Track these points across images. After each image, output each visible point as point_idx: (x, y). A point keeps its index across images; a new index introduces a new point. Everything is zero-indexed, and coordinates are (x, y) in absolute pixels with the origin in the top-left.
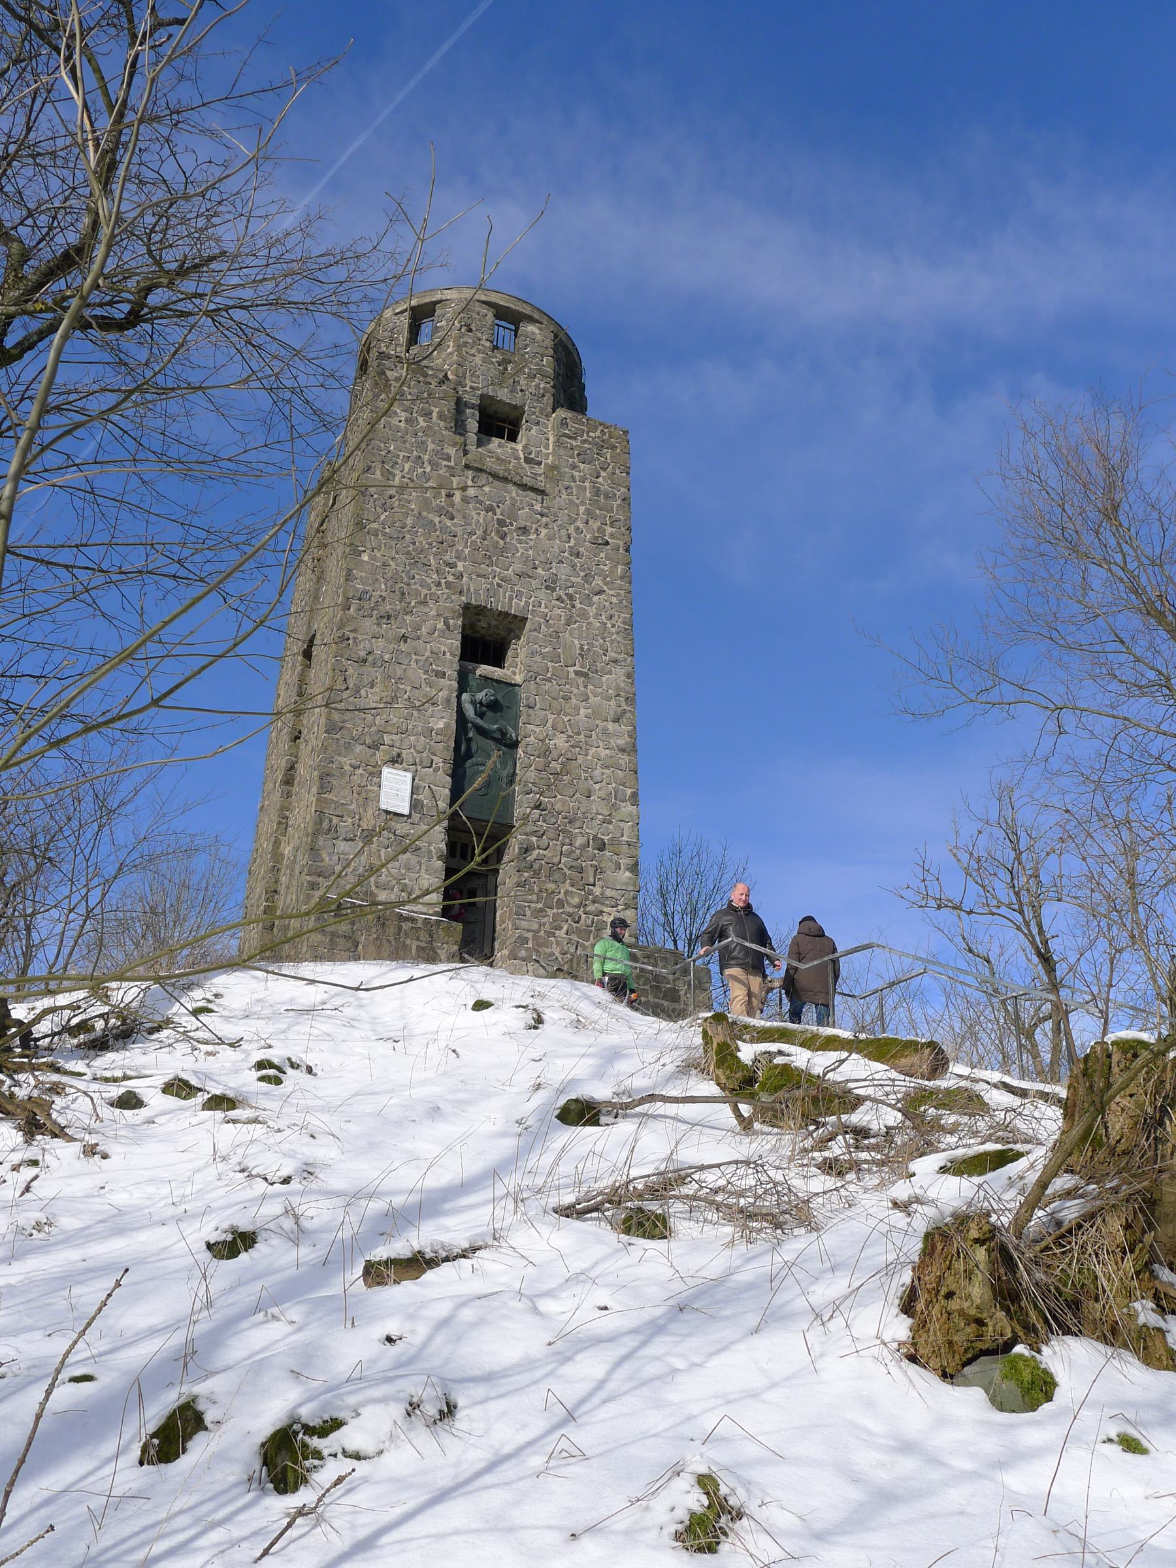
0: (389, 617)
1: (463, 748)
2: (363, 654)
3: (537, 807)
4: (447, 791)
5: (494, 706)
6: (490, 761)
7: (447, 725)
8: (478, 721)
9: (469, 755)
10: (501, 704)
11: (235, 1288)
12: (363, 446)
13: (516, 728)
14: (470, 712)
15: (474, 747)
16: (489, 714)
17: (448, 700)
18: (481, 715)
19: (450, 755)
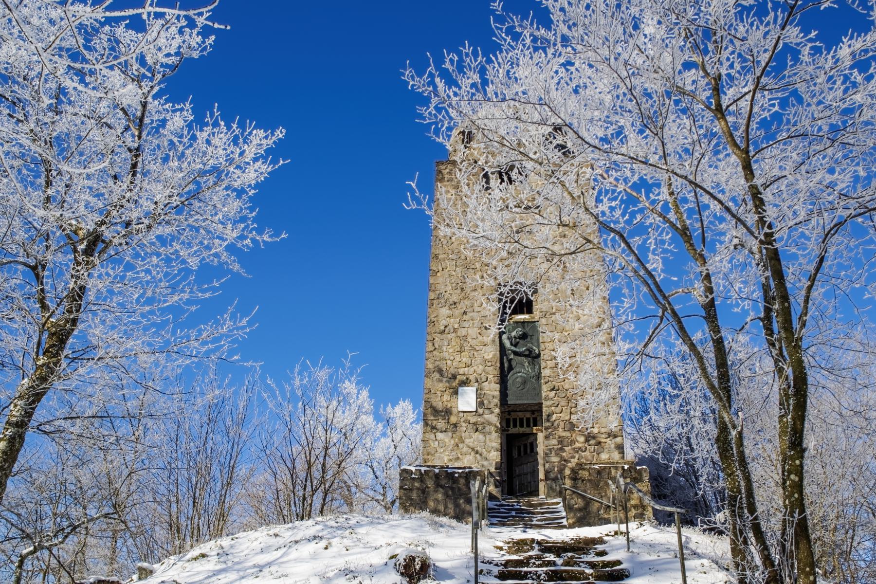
0: (455, 304)
1: (506, 365)
2: (442, 328)
3: (552, 390)
4: (498, 393)
5: (524, 336)
6: (522, 370)
7: (494, 356)
8: (513, 348)
9: (511, 368)
10: (528, 333)
11: (266, 565)
12: (223, 498)
13: (538, 346)
14: (507, 344)
15: (514, 363)
16: (521, 342)
17: (494, 341)
18: (516, 345)
19: (497, 372)
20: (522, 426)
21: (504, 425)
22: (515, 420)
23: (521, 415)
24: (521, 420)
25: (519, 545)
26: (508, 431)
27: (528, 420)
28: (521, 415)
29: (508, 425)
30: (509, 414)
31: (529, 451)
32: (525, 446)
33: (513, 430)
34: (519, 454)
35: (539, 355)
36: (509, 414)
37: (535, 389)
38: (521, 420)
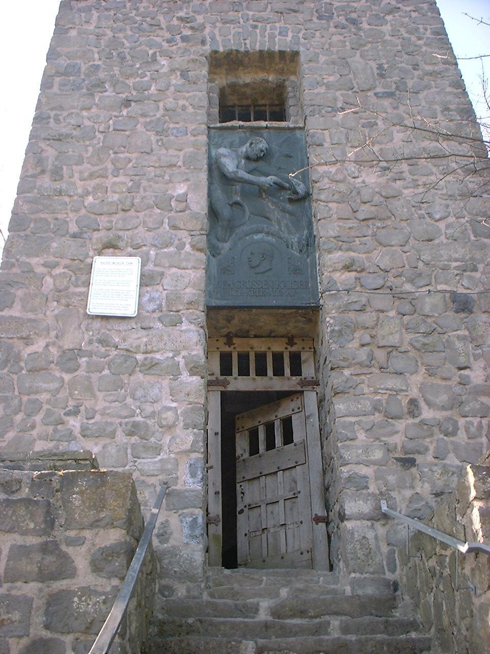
3: (348, 268)
20: (261, 372)
21: (216, 368)
22: (244, 358)
23: (259, 346)
24: (261, 358)
25: (254, 617)
26: (225, 384)
27: (278, 358)
28: (259, 346)
29: (226, 370)
30: (229, 343)
31: (262, 436)
32: (270, 428)
33: (239, 384)
34: (254, 450)
35: (307, 196)
36: (229, 343)
37: (297, 271)
38: (261, 358)
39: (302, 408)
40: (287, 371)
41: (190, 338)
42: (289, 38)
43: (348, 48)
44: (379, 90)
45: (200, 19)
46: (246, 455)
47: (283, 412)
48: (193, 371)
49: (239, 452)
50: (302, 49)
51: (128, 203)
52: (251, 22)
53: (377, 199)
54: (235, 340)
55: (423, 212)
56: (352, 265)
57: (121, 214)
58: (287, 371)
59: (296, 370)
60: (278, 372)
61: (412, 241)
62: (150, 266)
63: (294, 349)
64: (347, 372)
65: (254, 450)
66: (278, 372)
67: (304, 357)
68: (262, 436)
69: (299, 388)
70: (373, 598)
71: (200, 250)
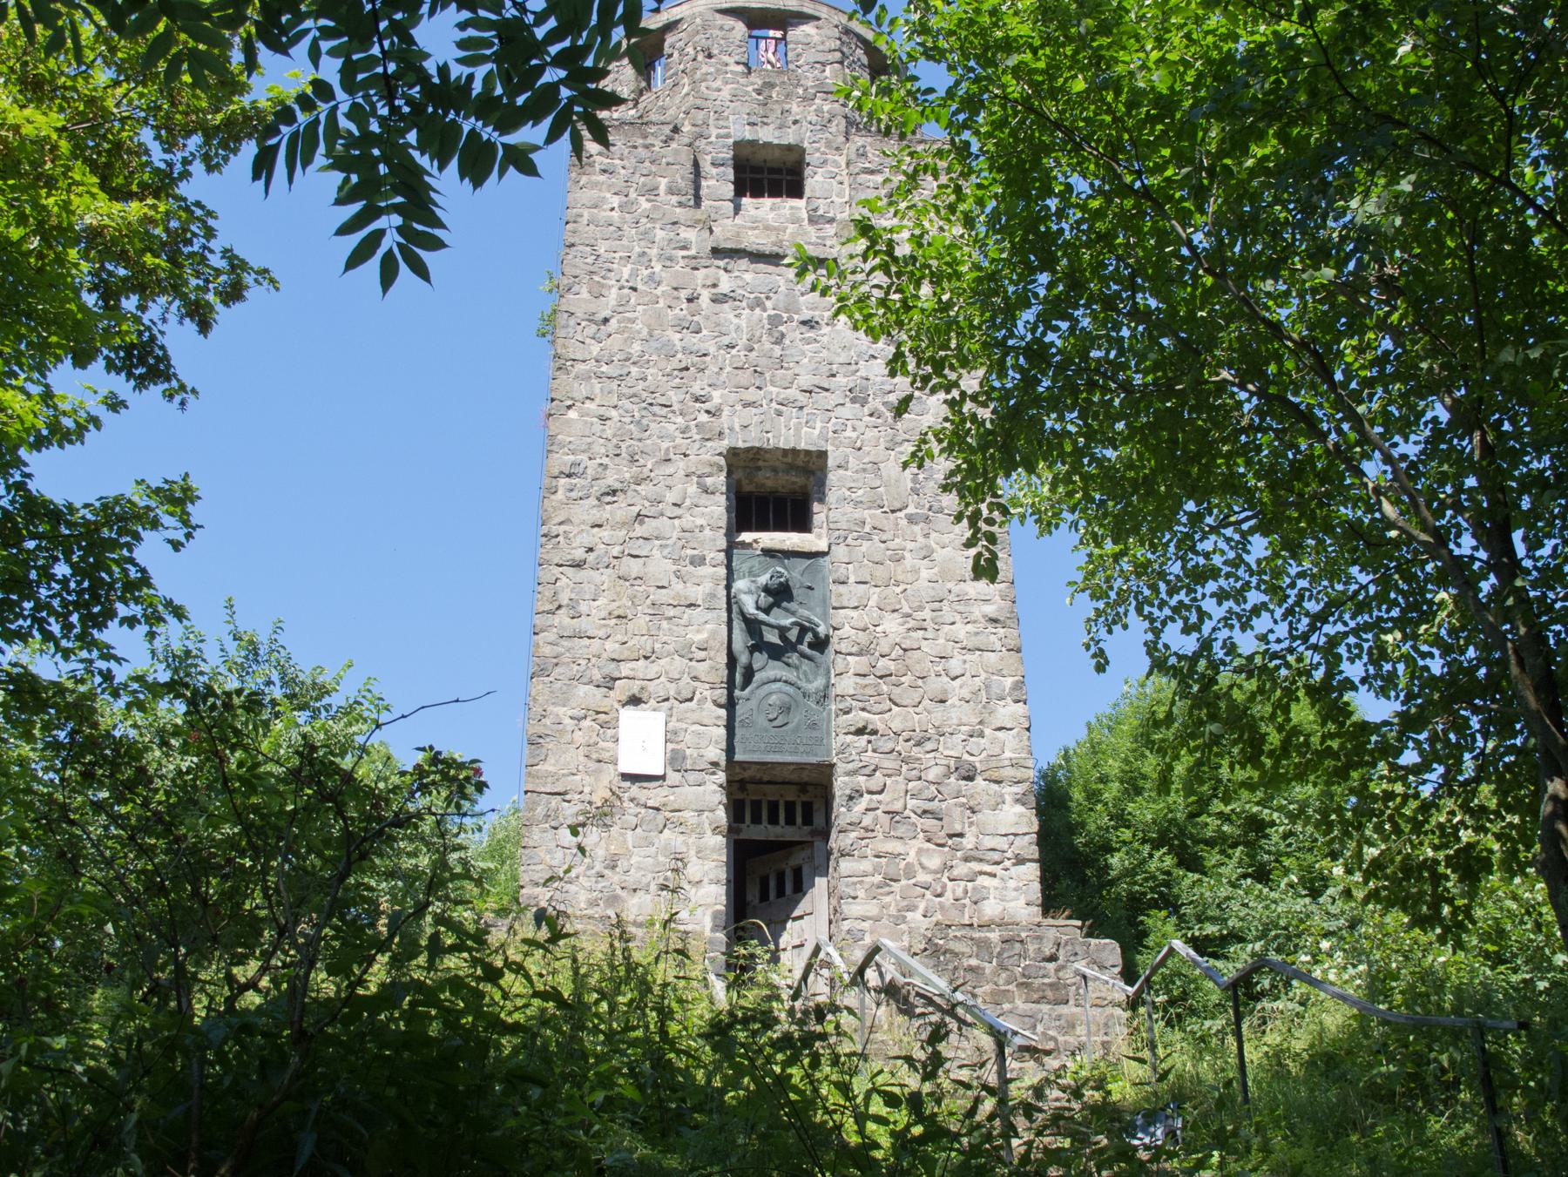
20: (773, 820)
31: (772, 884)
32: (781, 878)
34: (764, 897)
39: (812, 858)
40: (799, 820)
41: (711, 793)
42: (817, 432)
43: (882, 447)
44: (911, 510)
45: (717, 397)
46: (757, 901)
47: (795, 861)
48: (715, 830)
49: (749, 898)
50: (830, 448)
51: (649, 649)
52: (774, 405)
53: (897, 652)
54: (750, 787)
55: (940, 668)
56: (865, 727)
57: (642, 661)
58: (799, 820)
59: (808, 820)
60: (790, 821)
61: (926, 702)
62: (673, 725)
63: (805, 798)
64: (853, 835)
65: (764, 897)
66: (790, 821)
67: (815, 807)
68: (772, 884)
69: (809, 839)
70: (281, 739)
71: (720, 706)
